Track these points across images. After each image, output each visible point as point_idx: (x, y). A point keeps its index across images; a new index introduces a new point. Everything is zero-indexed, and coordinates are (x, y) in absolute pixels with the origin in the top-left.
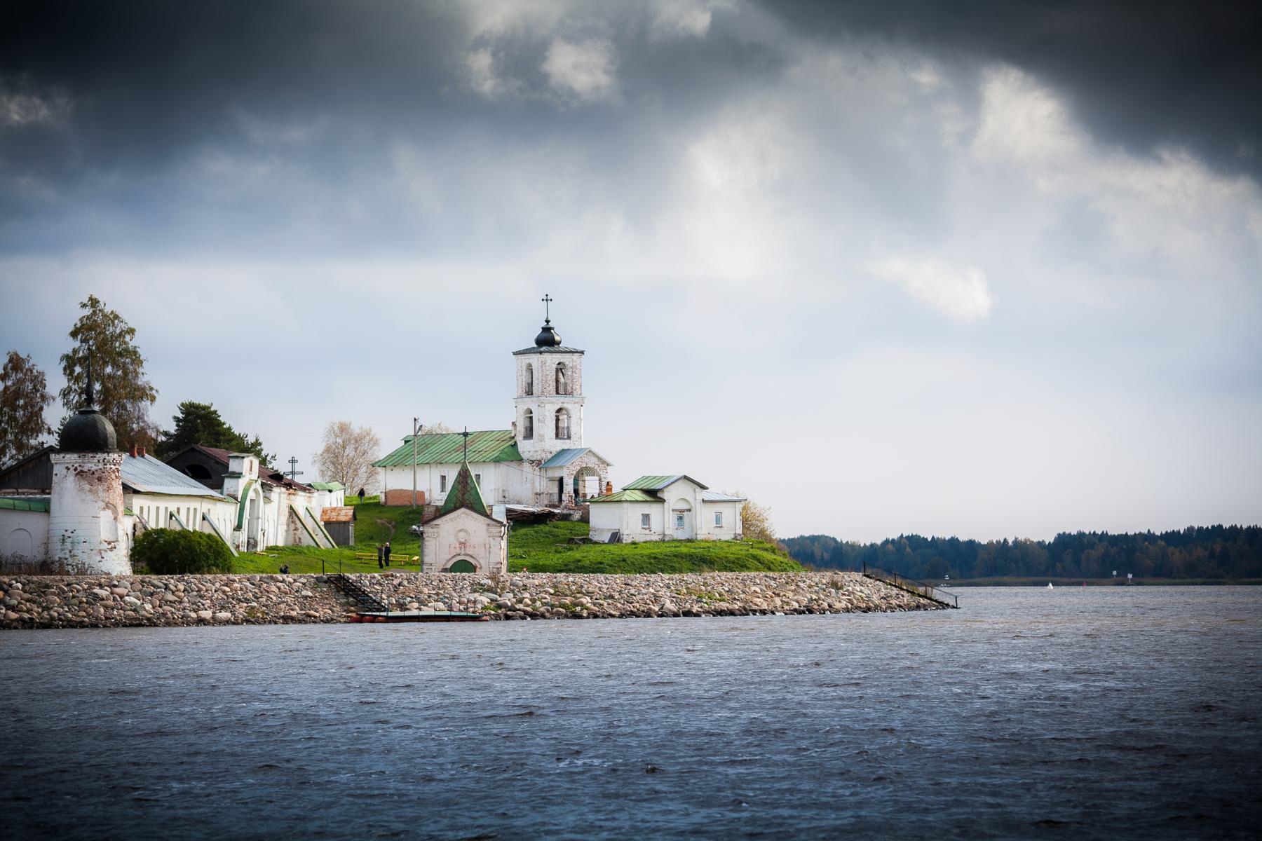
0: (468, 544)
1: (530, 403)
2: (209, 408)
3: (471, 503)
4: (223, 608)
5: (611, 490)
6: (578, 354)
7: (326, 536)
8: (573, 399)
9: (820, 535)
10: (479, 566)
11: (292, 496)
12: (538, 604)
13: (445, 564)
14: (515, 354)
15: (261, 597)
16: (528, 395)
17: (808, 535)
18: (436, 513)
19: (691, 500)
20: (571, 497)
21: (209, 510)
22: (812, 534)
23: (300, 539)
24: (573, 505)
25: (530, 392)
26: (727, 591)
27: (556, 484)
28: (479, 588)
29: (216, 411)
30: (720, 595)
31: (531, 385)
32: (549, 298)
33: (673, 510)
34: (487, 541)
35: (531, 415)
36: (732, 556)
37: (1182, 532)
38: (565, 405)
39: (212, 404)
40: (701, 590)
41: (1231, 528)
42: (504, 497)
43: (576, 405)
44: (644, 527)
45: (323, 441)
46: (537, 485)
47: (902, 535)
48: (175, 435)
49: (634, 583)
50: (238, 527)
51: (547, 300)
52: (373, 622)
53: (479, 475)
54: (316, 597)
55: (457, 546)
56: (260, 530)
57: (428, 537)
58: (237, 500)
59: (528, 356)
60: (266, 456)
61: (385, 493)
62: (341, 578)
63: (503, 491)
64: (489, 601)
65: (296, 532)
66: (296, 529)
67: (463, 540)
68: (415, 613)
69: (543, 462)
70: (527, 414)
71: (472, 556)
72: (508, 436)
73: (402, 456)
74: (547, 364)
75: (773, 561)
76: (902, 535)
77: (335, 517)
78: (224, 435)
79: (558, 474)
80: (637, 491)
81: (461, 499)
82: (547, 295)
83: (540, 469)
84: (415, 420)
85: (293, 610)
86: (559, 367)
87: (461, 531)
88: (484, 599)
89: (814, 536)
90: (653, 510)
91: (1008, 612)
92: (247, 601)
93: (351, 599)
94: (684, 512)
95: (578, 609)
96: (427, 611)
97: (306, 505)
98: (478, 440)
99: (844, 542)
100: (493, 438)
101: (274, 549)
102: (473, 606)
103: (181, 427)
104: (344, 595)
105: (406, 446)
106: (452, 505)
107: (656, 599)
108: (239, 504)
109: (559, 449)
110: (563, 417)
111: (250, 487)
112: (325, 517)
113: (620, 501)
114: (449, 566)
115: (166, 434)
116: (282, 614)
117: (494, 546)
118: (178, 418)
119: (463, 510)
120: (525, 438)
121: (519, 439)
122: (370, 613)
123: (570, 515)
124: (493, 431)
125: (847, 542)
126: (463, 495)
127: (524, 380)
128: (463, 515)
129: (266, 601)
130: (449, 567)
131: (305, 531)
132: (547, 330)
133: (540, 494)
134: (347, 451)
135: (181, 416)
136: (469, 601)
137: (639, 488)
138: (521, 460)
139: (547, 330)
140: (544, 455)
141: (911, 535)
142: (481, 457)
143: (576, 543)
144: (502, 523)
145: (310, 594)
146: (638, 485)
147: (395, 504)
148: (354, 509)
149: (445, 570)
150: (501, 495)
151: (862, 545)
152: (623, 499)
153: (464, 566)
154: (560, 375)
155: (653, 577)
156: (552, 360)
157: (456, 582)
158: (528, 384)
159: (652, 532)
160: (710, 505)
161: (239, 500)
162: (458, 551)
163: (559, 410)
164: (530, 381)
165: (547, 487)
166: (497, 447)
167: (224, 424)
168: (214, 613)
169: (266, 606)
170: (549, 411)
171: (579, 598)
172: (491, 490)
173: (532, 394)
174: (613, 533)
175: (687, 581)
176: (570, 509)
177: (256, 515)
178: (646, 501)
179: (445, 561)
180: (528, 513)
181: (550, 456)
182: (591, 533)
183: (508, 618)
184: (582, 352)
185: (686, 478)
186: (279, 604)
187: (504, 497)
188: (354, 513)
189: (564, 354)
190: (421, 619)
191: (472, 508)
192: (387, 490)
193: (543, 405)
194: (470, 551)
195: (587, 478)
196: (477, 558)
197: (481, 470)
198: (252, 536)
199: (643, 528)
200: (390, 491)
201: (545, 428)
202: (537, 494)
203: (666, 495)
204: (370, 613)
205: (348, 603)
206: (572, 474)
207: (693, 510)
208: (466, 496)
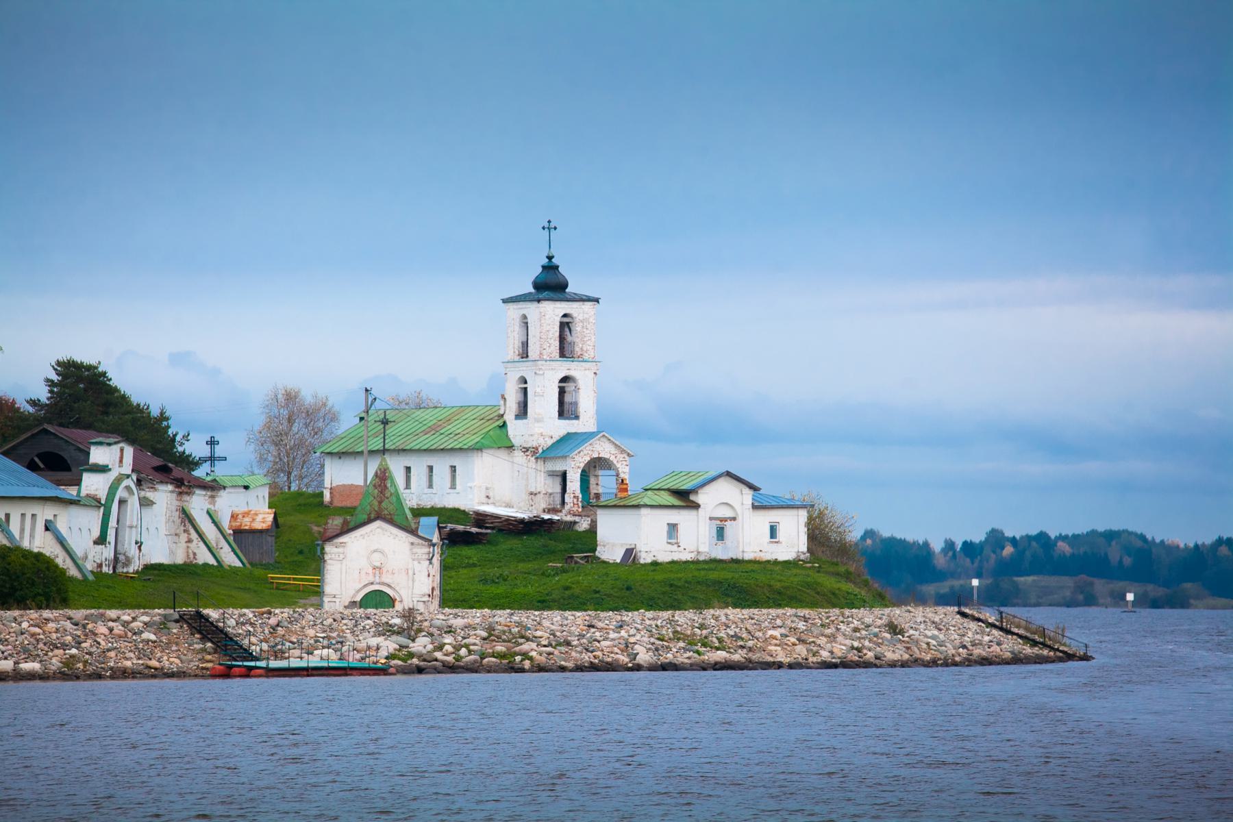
0: (384, 570)
1: (525, 369)
2: (96, 368)
3: (390, 514)
4: (30, 657)
5: (626, 490)
6: (591, 303)
7: (233, 550)
9: (1121, 529)
10: (398, 599)
11: (186, 498)
12: (463, 651)
13: (354, 595)
14: (505, 301)
15: (85, 642)
16: (522, 358)
17: (1103, 530)
18: (342, 527)
20: (577, 498)
21: (55, 516)
22: (1108, 528)
23: (195, 554)
24: (580, 510)
25: (524, 354)
26: (732, 636)
27: (558, 480)
28: (388, 630)
29: (105, 373)
30: (720, 640)
31: (525, 345)
32: (552, 225)
33: (711, 519)
34: (410, 566)
35: (525, 386)
36: (778, 584)
38: (572, 373)
39: (99, 363)
40: (694, 634)
43: (587, 372)
44: (669, 541)
45: (263, 413)
48: (47, 405)
49: (600, 625)
50: (101, 540)
51: (549, 228)
52: (247, 676)
53: (455, 467)
54: (161, 641)
55: (370, 570)
57: (330, 559)
58: (100, 502)
59: (522, 305)
60: (175, 436)
61: (331, 489)
62: (199, 615)
63: (487, 489)
64: (398, 647)
65: (189, 545)
66: (190, 541)
67: (378, 564)
68: (295, 663)
69: (540, 451)
70: (521, 383)
71: (389, 586)
72: (496, 414)
73: (352, 440)
75: (837, 592)
77: (249, 524)
78: (116, 406)
79: (559, 466)
80: (663, 492)
81: (376, 509)
82: (549, 222)
83: (537, 458)
84: (367, 390)
85: (127, 659)
86: (566, 320)
87: (375, 551)
88: (388, 645)
89: (1111, 531)
90: (683, 518)
91: (151, 801)
92: (65, 646)
93: (209, 644)
94: (726, 521)
95: (518, 658)
96: (314, 661)
97: (207, 506)
98: (456, 418)
99: (1158, 541)
100: (474, 417)
101: (155, 569)
102: (375, 654)
103: (56, 393)
104: (201, 639)
106: (365, 517)
107: (627, 647)
108: (102, 509)
109: (563, 432)
110: (569, 387)
111: (119, 485)
112: (234, 524)
113: (637, 507)
114: (358, 599)
115: (33, 403)
116: (112, 664)
117: (420, 571)
118: (52, 381)
119: (378, 523)
120: (518, 417)
121: (509, 417)
122: (240, 663)
123: (575, 523)
124: (478, 406)
125: (1162, 542)
126: (380, 503)
128: (379, 530)
129: (91, 646)
130: (359, 600)
131: (201, 544)
132: (550, 267)
133: (536, 494)
134: (295, 429)
135: (55, 378)
136: (369, 648)
137: (666, 487)
138: (511, 448)
139: (550, 267)
140: (541, 441)
142: (460, 440)
143: (576, 562)
144: (431, 541)
145: (153, 637)
146: (654, 484)
147: (344, 504)
148: (275, 514)
149: (353, 604)
151: (1182, 546)
152: (642, 503)
153: (378, 599)
154: (567, 329)
155: (628, 616)
156: (552, 311)
157: (356, 621)
158: (523, 343)
159: (681, 548)
161: (103, 502)
162: (371, 579)
163: (565, 379)
164: (526, 340)
166: (478, 429)
168: (16, 663)
169: (90, 654)
171: (521, 644)
173: (527, 356)
174: (627, 549)
175: (678, 621)
176: (574, 515)
178: (673, 507)
179: (354, 592)
180: (515, 521)
181: (550, 442)
182: (598, 549)
183: (420, 670)
184: (597, 300)
185: (729, 474)
186: (109, 650)
188: (275, 518)
190: (310, 672)
191: (391, 521)
192: (334, 485)
193: (541, 372)
194: (386, 579)
195: (600, 472)
196: (397, 589)
198: (122, 551)
199: (669, 543)
200: (337, 486)
201: (544, 402)
202: (531, 494)
203: (701, 498)
204: (240, 663)
205: (204, 650)
206: (579, 467)
207: (740, 518)
208: (384, 505)
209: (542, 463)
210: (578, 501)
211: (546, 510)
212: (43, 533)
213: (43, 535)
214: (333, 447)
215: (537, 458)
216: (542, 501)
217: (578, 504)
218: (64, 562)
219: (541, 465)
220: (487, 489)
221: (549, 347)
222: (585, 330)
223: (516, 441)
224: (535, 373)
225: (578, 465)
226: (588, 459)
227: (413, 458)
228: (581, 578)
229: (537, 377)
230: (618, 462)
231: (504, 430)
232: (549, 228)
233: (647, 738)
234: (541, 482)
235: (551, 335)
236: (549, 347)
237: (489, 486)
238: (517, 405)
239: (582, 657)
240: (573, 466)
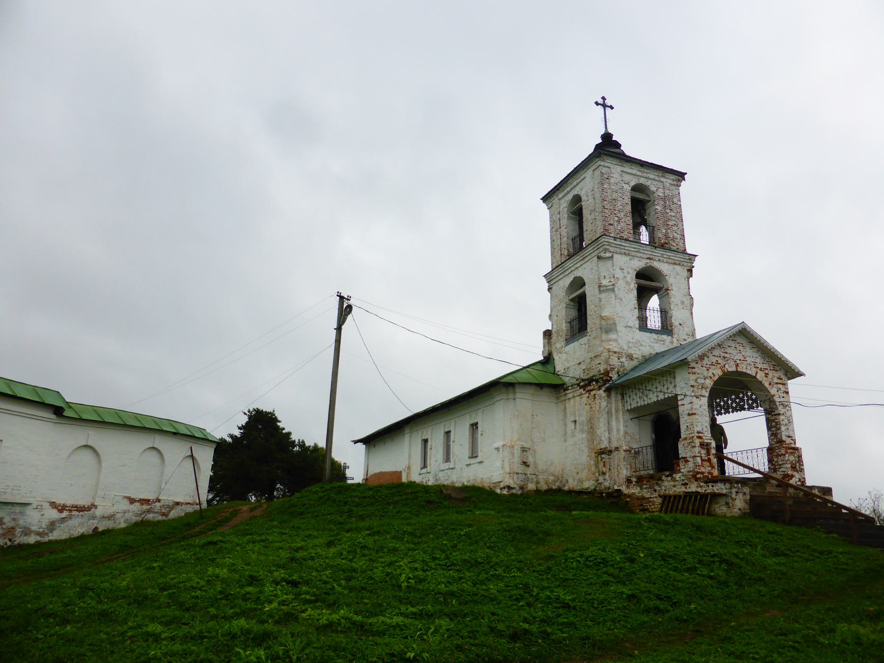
20: (705, 446)
32: (601, 101)
37: (212, 474)
38: (656, 264)
41: (213, 461)
42: (525, 464)
46: (601, 430)
47: (684, 180)
63: (524, 450)
74: (612, 180)
76: (684, 180)
82: (603, 98)
127: (564, 233)
132: (607, 138)
150: (517, 460)
165: (626, 433)
167: (284, 429)
170: (621, 269)
172: (498, 449)
187: (525, 464)
197: (429, 432)
202: (602, 452)
203: (98, 507)
209: (620, 397)
210: (708, 453)
211: (634, 479)
215: (608, 391)
216: (622, 464)
217: (709, 460)
219: (616, 401)
220: (524, 450)
221: (618, 222)
222: (668, 211)
224: (599, 258)
225: (701, 381)
226: (718, 373)
227: (480, 411)
228: (693, 606)
229: (601, 263)
230: (770, 384)
231: (549, 368)
232: (604, 104)
233: (742, 559)
234: (618, 430)
235: (656, 338)
236: (618, 222)
237: (526, 445)
238: (568, 325)
239: (684, 416)
240: (693, 383)
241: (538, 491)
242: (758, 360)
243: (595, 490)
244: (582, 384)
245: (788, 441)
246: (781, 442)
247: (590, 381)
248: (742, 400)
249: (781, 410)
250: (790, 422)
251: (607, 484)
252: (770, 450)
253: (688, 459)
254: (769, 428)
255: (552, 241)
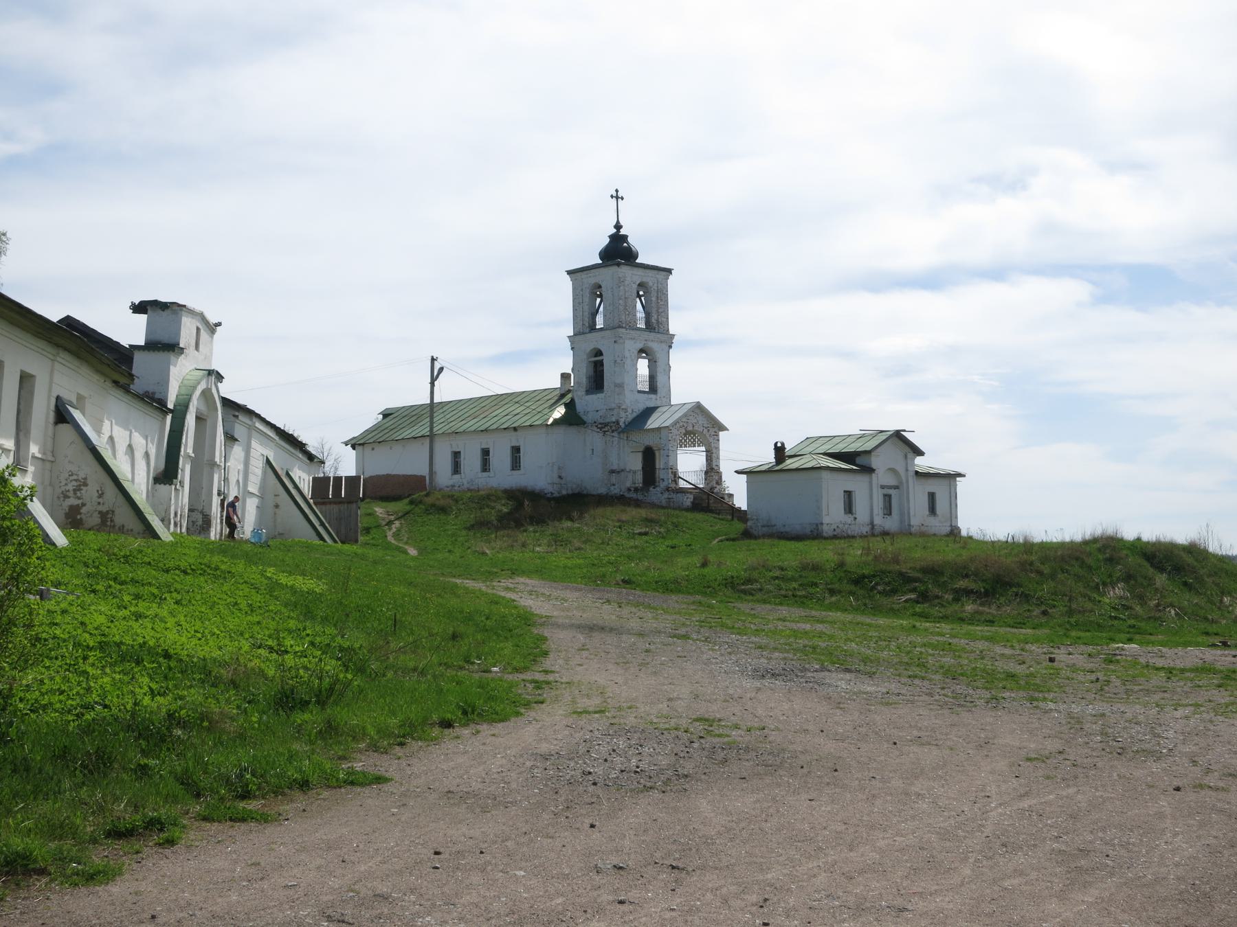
8: (659, 335)
19: (902, 471)
38: (651, 344)
50: (167, 475)
56: (215, 492)
63: (559, 468)
82: (617, 191)
105: (385, 421)
108: (169, 417)
139: (618, 226)
141: (1010, 539)
150: (556, 476)
160: (923, 480)
161: (170, 406)
177: (206, 457)
187: (560, 477)
189: (648, 271)
193: (621, 341)
202: (613, 472)
211: (632, 489)
212: (51, 427)
213: (50, 432)
214: (407, 433)
218: (100, 496)
223: (588, 418)
232: (617, 197)
241: (568, 495)
242: (705, 422)
243: (607, 494)
244: (600, 426)
245: (716, 468)
246: (712, 469)
247: (606, 425)
248: (694, 440)
249: (714, 451)
250: (718, 458)
251: (616, 491)
252: (706, 473)
253: (413, 506)
254: (707, 460)
255: (575, 310)
